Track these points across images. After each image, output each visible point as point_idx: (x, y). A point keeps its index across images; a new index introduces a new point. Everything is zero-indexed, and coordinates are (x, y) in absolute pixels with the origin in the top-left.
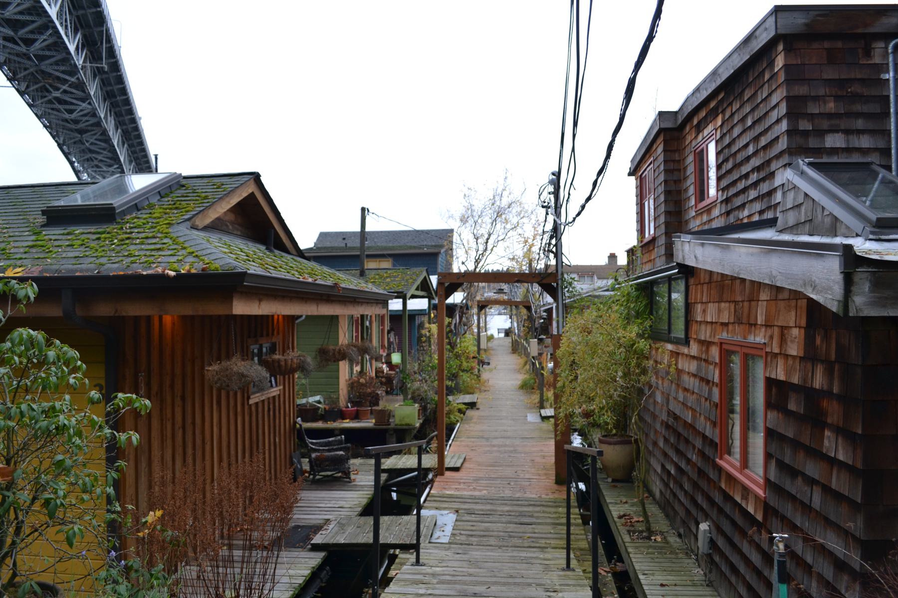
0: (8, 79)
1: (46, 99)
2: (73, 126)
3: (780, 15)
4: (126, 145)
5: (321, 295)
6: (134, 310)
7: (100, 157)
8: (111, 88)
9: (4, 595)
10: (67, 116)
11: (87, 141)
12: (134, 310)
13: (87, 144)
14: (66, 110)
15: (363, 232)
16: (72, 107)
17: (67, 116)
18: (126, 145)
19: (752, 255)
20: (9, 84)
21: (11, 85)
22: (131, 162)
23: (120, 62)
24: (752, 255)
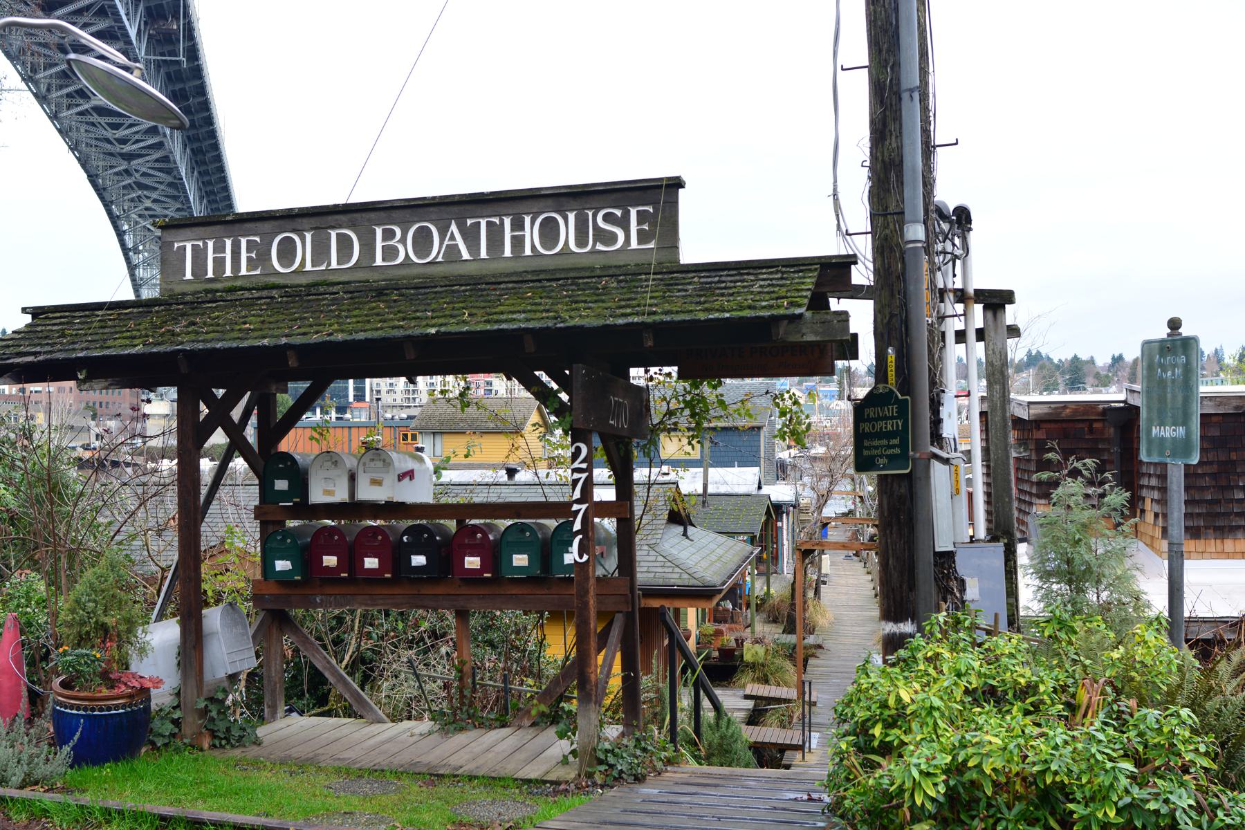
0: (23, 79)
1: (76, 110)
2: (118, 148)
3: (1031, 406)
4: (196, 173)
5: (921, 69)
6: (655, 603)
7: (154, 195)
8: (181, 86)
9: (757, 464)
10: (110, 134)
11: (137, 171)
12: (655, 603)
13: (137, 175)
14: (108, 124)
15: (934, 147)
16: (157, 165)
17: (110, 134)
18: (196, 173)
19: (1145, 593)
20: (23, 86)
21: (27, 89)
22: (201, 198)
23: (199, 46)
24: (1145, 593)
